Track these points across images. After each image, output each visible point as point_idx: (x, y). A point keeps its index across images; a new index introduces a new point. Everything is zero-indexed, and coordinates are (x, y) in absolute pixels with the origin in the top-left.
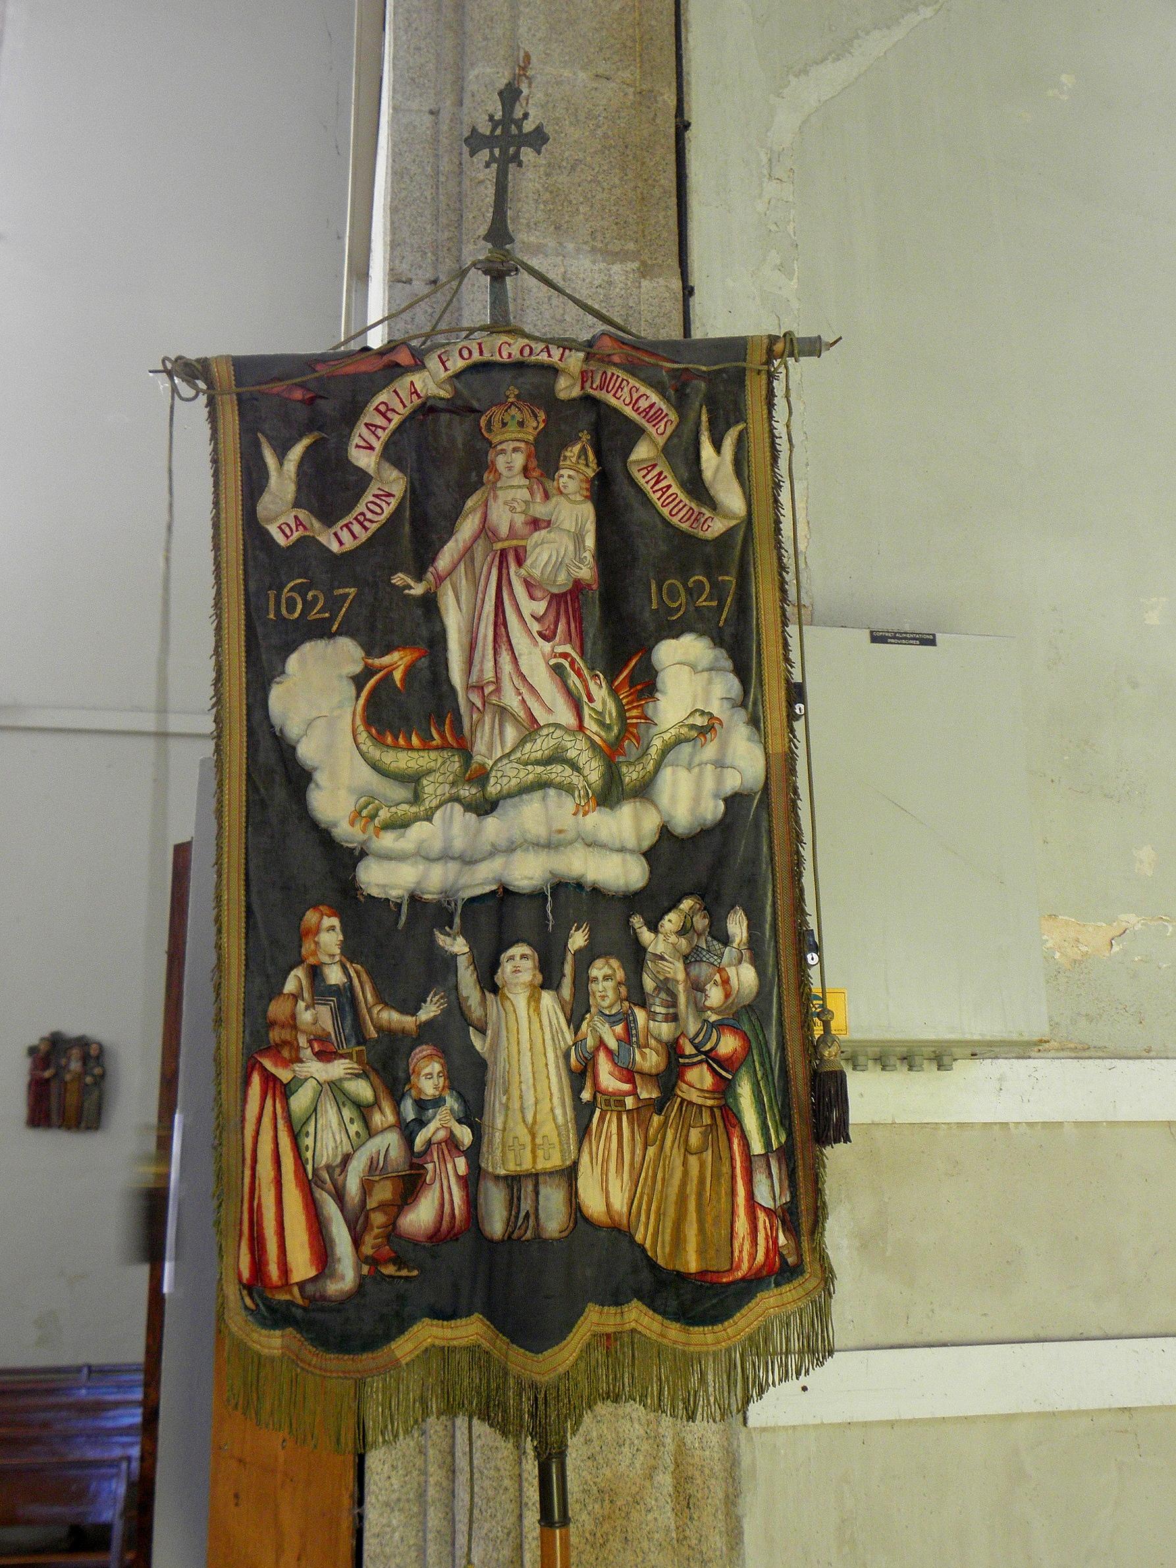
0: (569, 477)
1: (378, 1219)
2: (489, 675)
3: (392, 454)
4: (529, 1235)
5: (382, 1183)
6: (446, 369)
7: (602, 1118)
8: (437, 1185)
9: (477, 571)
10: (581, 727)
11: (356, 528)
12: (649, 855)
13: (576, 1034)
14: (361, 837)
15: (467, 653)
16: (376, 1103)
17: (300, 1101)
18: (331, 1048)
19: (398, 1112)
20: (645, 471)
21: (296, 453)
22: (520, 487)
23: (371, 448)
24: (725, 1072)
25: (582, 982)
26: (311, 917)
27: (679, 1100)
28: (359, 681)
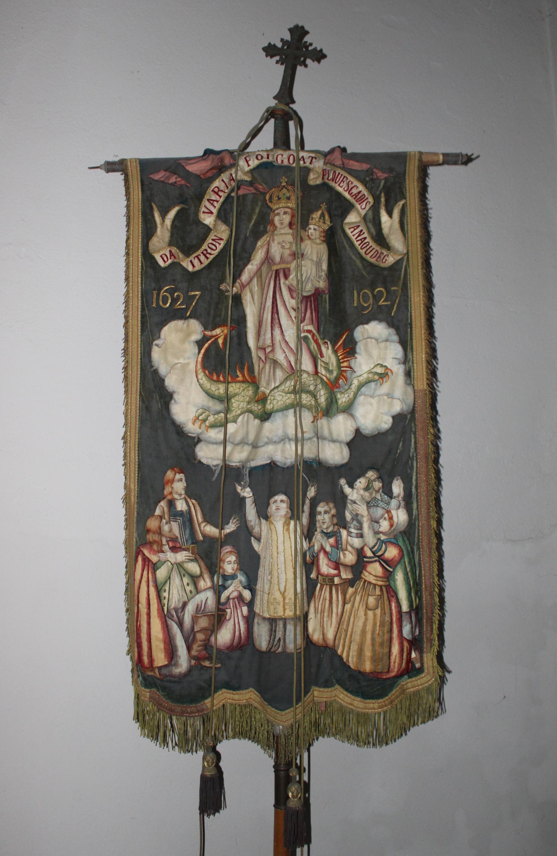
0: (314, 229)
1: (200, 636)
2: (269, 342)
3: (223, 215)
4: (280, 650)
5: (203, 618)
6: (249, 166)
7: (321, 589)
8: (232, 621)
9: (263, 281)
10: (316, 373)
11: (202, 258)
12: (350, 444)
13: (310, 543)
14: (199, 431)
15: (258, 328)
16: (201, 575)
17: (161, 573)
18: (178, 545)
19: (212, 581)
20: (352, 230)
21: (172, 214)
22: (286, 234)
23: (211, 213)
24: (388, 566)
25: (313, 514)
26: (170, 474)
27: (363, 580)
28: (200, 344)
